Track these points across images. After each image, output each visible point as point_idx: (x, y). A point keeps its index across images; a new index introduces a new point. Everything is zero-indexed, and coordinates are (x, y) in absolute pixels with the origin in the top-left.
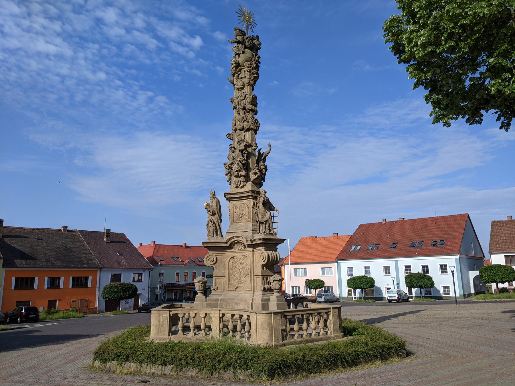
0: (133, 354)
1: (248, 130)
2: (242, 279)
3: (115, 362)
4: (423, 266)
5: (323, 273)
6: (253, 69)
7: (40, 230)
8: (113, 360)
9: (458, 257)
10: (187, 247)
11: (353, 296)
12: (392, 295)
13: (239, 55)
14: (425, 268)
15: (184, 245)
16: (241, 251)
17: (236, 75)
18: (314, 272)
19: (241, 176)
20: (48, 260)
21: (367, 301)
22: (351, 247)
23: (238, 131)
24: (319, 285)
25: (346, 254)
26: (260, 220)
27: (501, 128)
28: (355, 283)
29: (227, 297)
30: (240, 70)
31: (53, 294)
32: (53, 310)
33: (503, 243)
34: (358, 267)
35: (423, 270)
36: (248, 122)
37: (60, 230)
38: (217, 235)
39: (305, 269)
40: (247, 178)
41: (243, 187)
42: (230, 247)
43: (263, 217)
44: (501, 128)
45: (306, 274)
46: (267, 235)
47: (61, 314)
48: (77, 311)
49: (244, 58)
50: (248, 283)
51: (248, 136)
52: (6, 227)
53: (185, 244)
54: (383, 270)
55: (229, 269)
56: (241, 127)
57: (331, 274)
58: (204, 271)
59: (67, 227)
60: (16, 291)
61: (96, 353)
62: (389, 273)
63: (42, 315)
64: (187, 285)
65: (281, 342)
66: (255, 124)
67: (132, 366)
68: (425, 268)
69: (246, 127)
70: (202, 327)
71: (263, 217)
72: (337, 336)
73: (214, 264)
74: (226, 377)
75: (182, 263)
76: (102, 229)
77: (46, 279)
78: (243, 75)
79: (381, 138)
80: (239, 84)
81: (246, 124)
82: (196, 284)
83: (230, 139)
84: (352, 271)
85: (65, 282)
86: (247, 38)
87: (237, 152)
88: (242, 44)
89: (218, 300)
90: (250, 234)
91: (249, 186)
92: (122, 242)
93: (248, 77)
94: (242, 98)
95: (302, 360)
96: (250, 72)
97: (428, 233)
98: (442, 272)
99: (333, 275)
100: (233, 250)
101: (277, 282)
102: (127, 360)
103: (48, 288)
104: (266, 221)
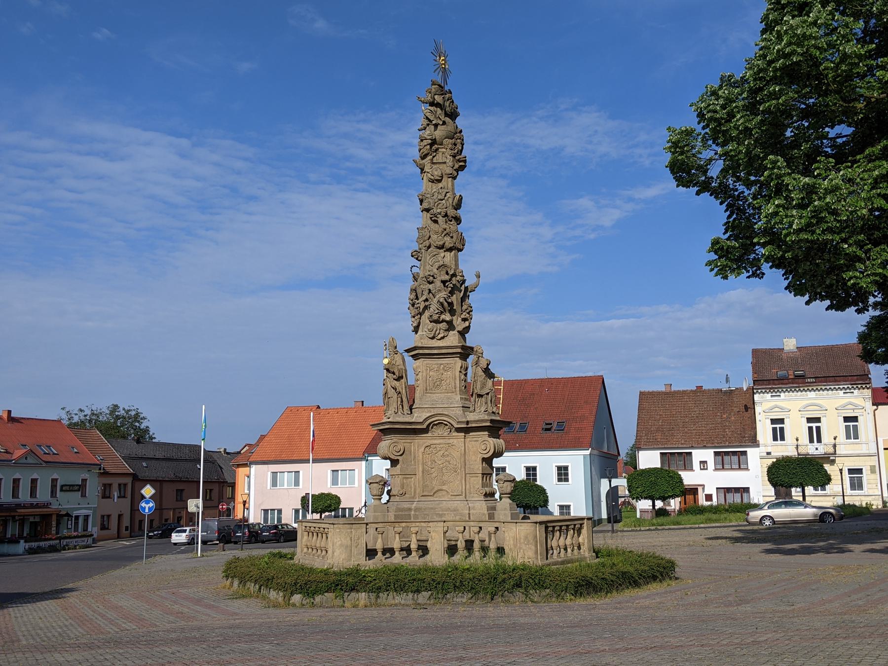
1: (450, 250)
2: (445, 478)
4: (528, 469)
5: (335, 482)
8: (327, 592)
9: (588, 452)
10: (12, 419)
13: (436, 126)
14: (531, 471)
15: (5, 416)
16: (442, 437)
18: (316, 478)
19: (443, 321)
24: (330, 506)
26: (478, 391)
29: (421, 505)
30: (437, 150)
33: (657, 430)
35: (528, 475)
36: (452, 237)
40: (451, 326)
41: (443, 338)
42: (425, 431)
43: (482, 388)
45: (297, 483)
49: (444, 133)
51: (449, 257)
53: (9, 412)
55: (423, 464)
56: (441, 243)
57: (352, 482)
58: (55, 476)
64: (19, 506)
68: (531, 471)
69: (448, 245)
70: (414, 546)
71: (482, 388)
73: (401, 455)
75: (7, 456)
78: (439, 158)
79: (356, 190)
80: (436, 173)
81: (447, 239)
83: (417, 259)
88: (442, 109)
90: (459, 412)
93: (451, 164)
96: (454, 156)
97: (536, 408)
98: (560, 480)
99: (356, 485)
100: (430, 434)
101: (509, 483)
104: (488, 394)
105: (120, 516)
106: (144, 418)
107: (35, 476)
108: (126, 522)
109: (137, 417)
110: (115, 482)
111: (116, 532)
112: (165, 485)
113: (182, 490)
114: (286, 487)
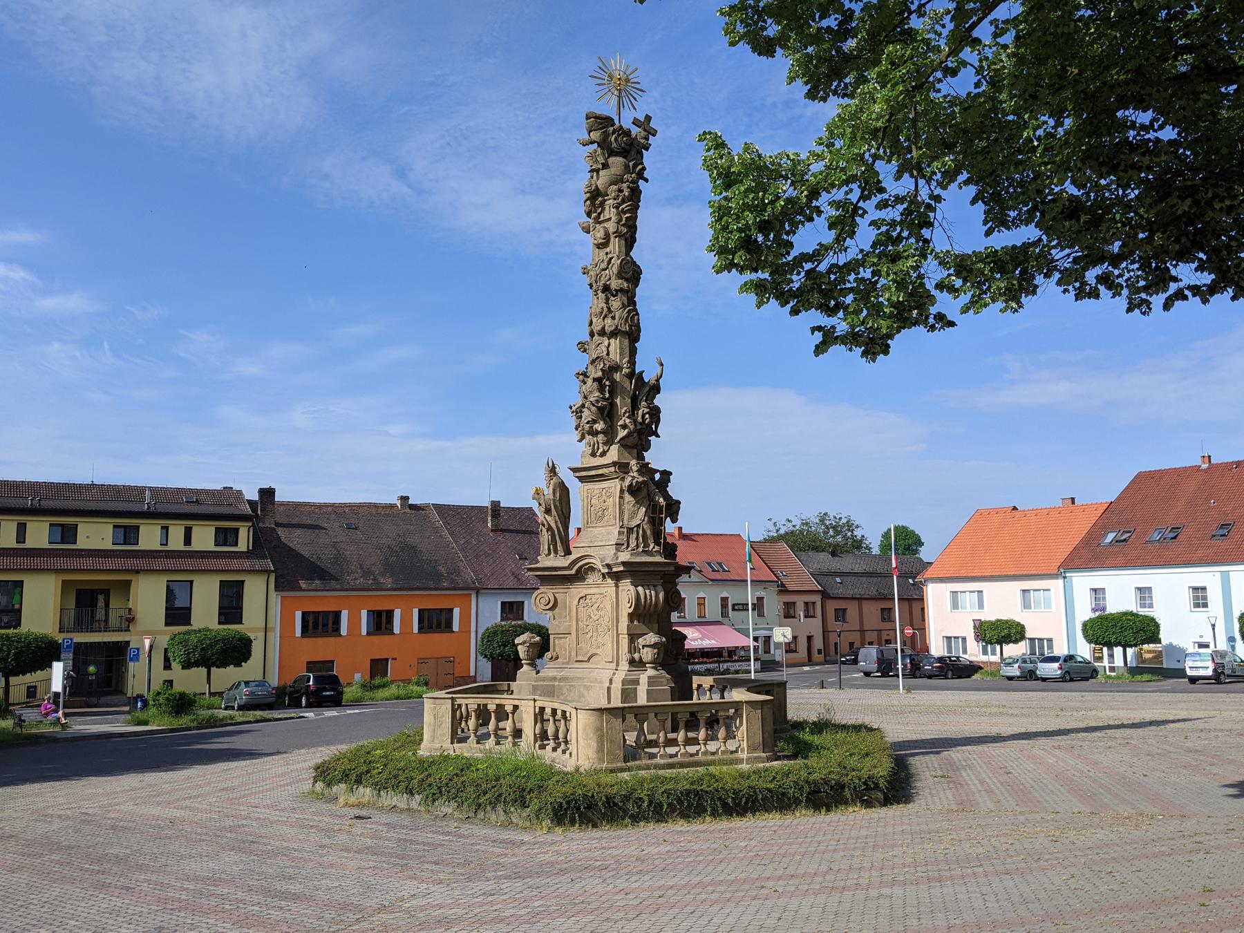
0: (368, 772)
2: (600, 639)
3: (343, 786)
5: (1026, 605)
6: (623, 201)
7: (351, 506)
11: (1106, 663)
12: (1199, 664)
15: (676, 533)
17: (594, 215)
18: (1001, 600)
20: (367, 573)
21: (1138, 677)
22: (1105, 535)
23: (596, 337)
24: (1009, 635)
25: (1089, 554)
27: (1129, 310)
28: (1109, 630)
30: (602, 204)
31: (381, 647)
32: (377, 681)
34: (1120, 590)
36: (613, 318)
37: (393, 506)
38: (556, 552)
39: (980, 592)
41: (604, 454)
43: (631, 518)
44: (1129, 310)
45: (981, 606)
46: (638, 554)
47: (393, 690)
48: (426, 684)
50: (607, 651)
52: (282, 504)
54: (1186, 598)
56: (599, 328)
57: (1048, 604)
58: (725, 595)
59: (407, 498)
60: (306, 640)
61: (317, 768)
62: (1205, 605)
63: (349, 693)
65: (621, 764)
66: (626, 321)
67: (365, 793)
69: (608, 330)
71: (631, 518)
72: (756, 758)
74: (494, 817)
76: (480, 498)
77: (364, 613)
80: (598, 235)
82: (519, 647)
84: (1104, 599)
85: (405, 619)
86: (614, 132)
87: (589, 382)
89: (555, 679)
90: (612, 550)
91: (613, 454)
92: (524, 532)
94: (603, 265)
95: (627, 798)
96: (617, 208)
99: (1054, 609)
102: (359, 781)
103: (368, 633)
104: (638, 526)
105: (809, 638)
106: (857, 527)
107: (702, 595)
108: (818, 643)
109: (850, 526)
110: (800, 601)
111: (805, 655)
112: (864, 603)
113: (845, 610)
114: (968, 609)
